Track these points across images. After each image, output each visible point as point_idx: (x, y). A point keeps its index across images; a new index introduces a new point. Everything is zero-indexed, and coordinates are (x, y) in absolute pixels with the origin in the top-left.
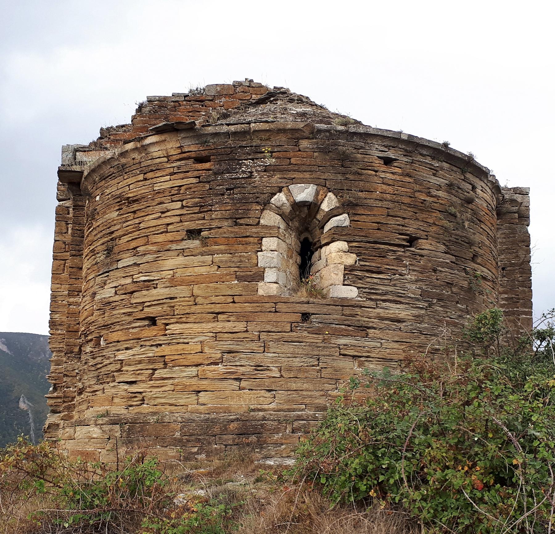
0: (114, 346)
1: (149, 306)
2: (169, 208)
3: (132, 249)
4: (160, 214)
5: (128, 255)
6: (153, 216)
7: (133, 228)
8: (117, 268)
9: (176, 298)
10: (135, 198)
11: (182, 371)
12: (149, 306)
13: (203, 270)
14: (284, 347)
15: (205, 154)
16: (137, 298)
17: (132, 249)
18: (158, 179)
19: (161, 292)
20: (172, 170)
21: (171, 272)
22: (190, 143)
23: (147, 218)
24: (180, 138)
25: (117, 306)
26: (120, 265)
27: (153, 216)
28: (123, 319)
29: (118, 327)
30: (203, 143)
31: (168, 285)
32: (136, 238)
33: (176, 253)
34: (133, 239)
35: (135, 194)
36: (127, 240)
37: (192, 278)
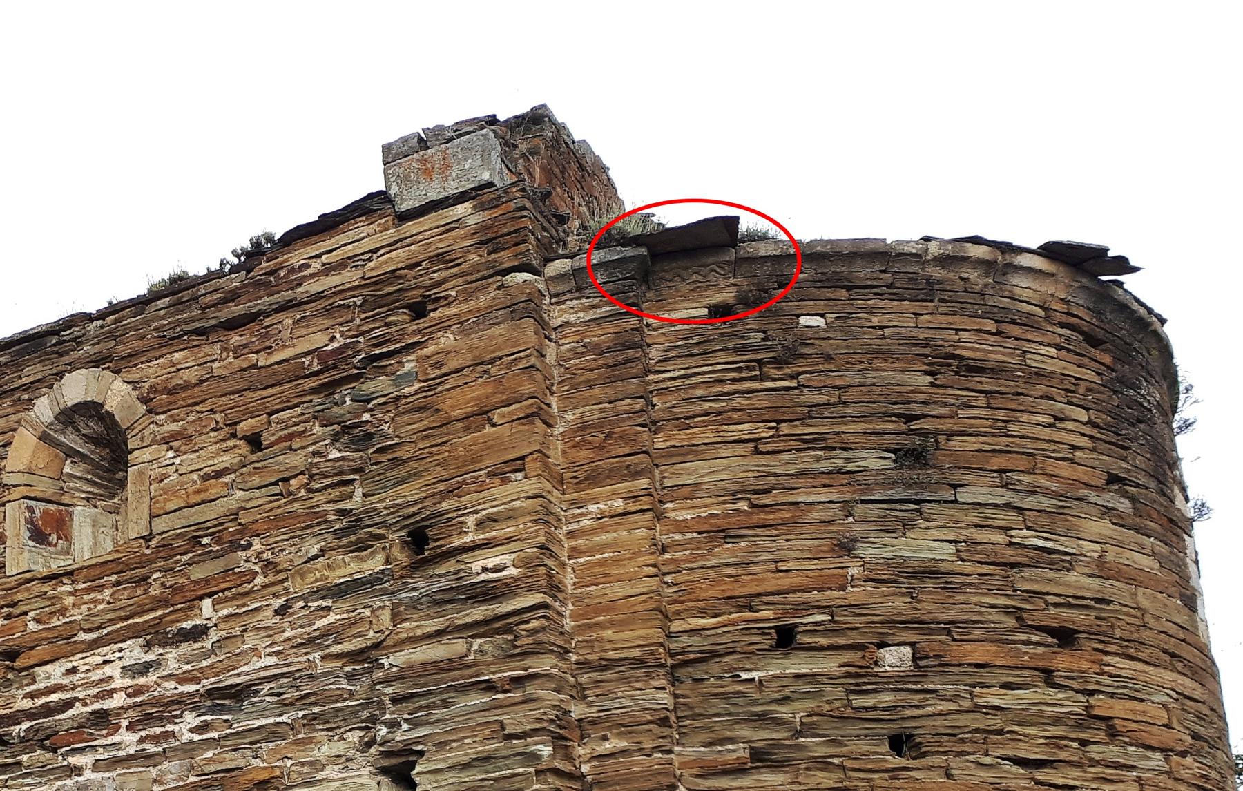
0: (965, 673)
1: (1056, 605)
2: (1067, 413)
3: (995, 471)
4: (1052, 420)
5: (986, 480)
6: (1040, 419)
7: (991, 427)
8: (956, 501)
9: (1109, 602)
10: (980, 364)
11: (1148, 758)
12: (1056, 605)
13: (1145, 562)
14: (126, 653)
15: (1100, 334)
16: (1028, 580)
17: (995, 471)
18: (1033, 345)
19: (1079, 581)
20: (1058, 340)
21: (1098, 547)
22: (1081, 302)
23: (1025, 418)
24: (1076, 284)
25: (964, 584)
26: (964, 495)
27: (1040, 419)
28: (990, 617)
29: (977, 634)
30: (1098, 313)
31: (1095, 572)
32: (1000, 451)
33: (1094, 510)
34: (993, 451)
35: (978, 355)
36: (976, 447)
37: (1133, 573)
